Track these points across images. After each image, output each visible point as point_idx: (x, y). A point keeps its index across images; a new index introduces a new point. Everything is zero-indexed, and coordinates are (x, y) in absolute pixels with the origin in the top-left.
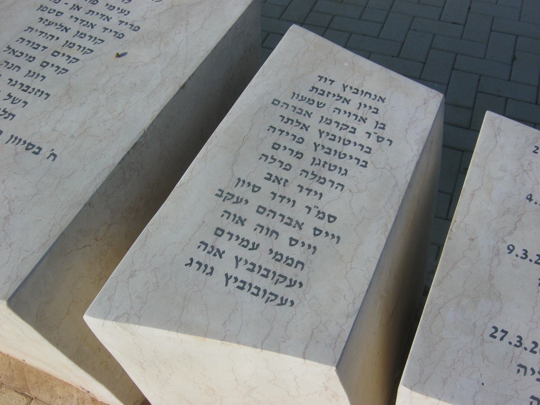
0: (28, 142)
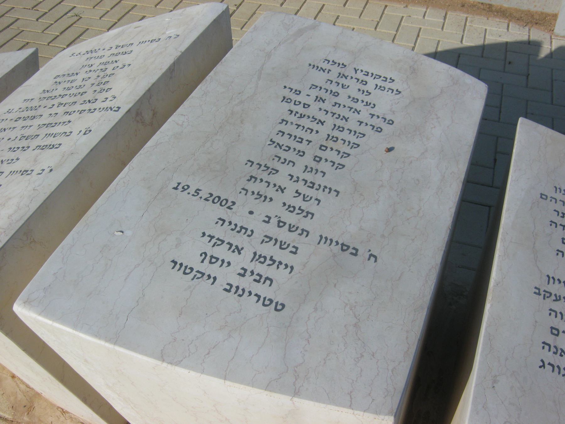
0: (340, 242)
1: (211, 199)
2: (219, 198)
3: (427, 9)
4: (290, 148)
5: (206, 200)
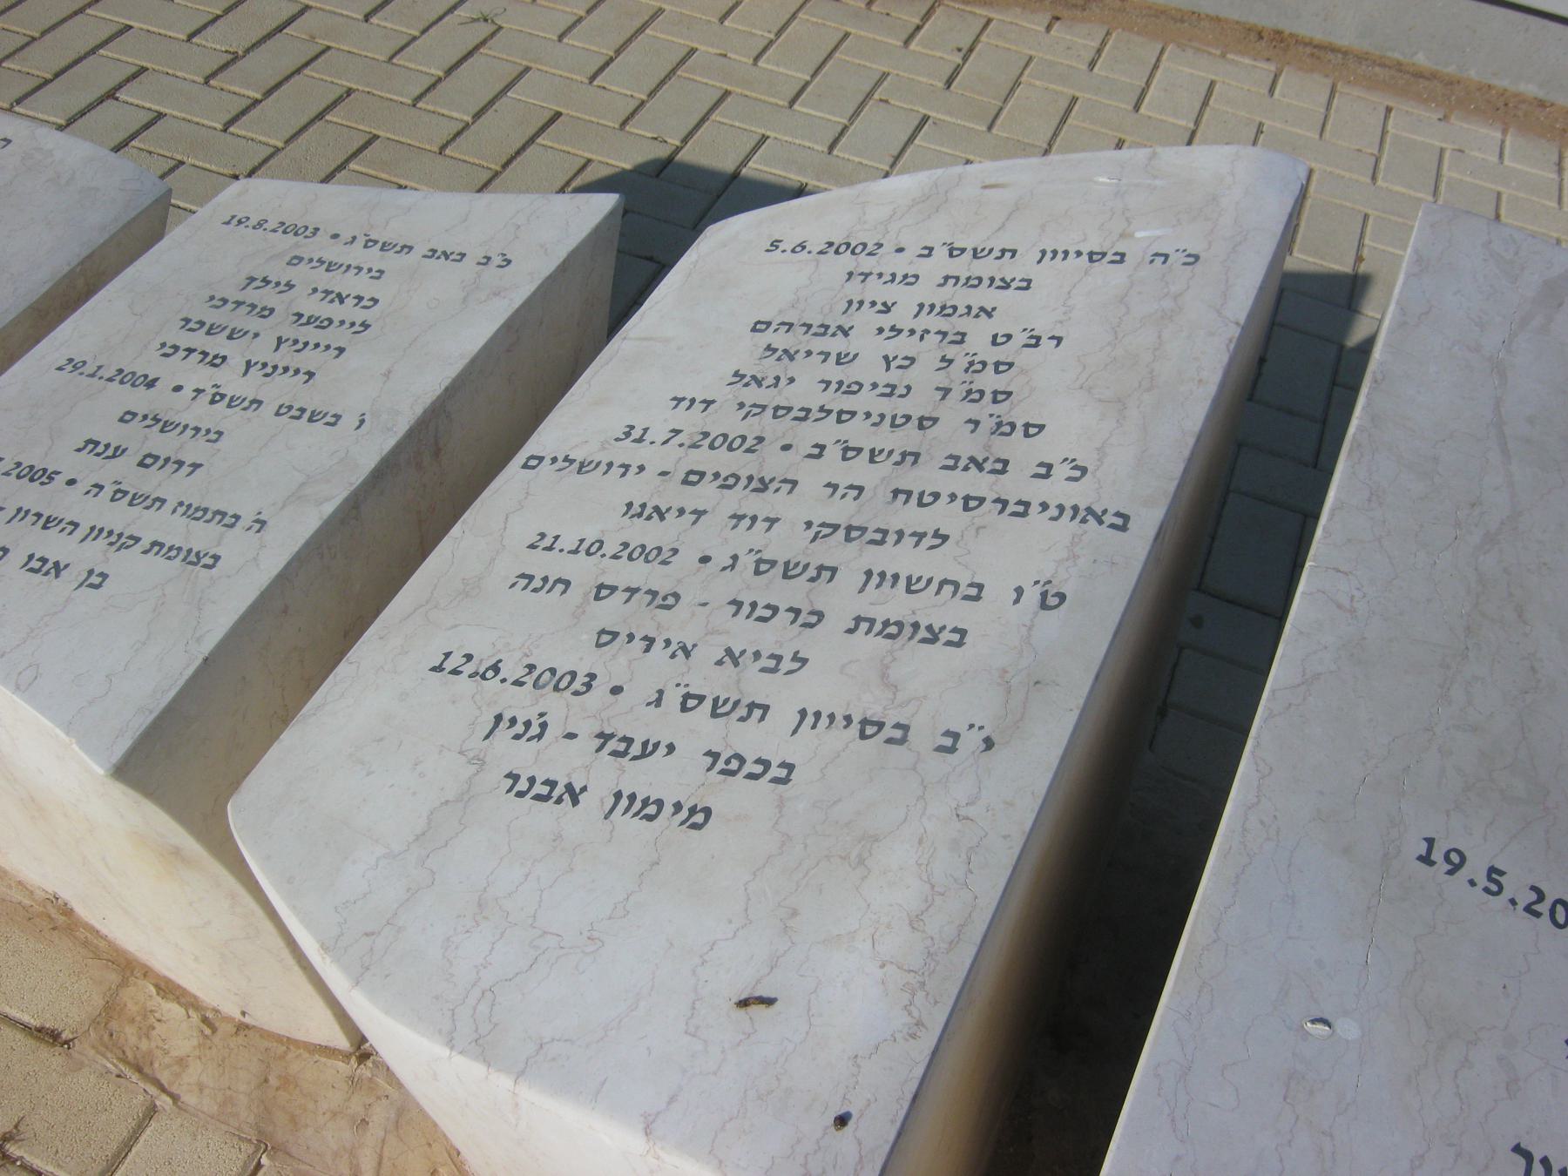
1: (625, 554)
2: (643, 547)
3: (1505, 132)
4: (1027, 505)
5: (615, 557)
